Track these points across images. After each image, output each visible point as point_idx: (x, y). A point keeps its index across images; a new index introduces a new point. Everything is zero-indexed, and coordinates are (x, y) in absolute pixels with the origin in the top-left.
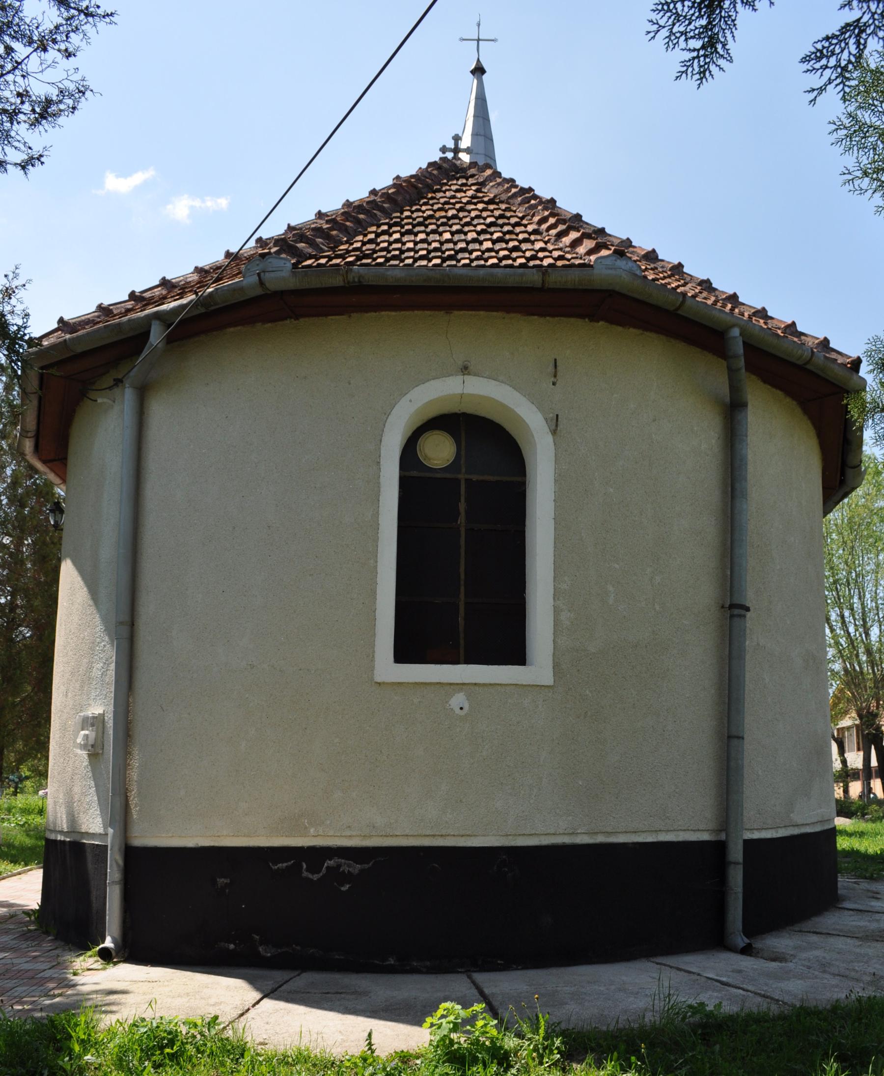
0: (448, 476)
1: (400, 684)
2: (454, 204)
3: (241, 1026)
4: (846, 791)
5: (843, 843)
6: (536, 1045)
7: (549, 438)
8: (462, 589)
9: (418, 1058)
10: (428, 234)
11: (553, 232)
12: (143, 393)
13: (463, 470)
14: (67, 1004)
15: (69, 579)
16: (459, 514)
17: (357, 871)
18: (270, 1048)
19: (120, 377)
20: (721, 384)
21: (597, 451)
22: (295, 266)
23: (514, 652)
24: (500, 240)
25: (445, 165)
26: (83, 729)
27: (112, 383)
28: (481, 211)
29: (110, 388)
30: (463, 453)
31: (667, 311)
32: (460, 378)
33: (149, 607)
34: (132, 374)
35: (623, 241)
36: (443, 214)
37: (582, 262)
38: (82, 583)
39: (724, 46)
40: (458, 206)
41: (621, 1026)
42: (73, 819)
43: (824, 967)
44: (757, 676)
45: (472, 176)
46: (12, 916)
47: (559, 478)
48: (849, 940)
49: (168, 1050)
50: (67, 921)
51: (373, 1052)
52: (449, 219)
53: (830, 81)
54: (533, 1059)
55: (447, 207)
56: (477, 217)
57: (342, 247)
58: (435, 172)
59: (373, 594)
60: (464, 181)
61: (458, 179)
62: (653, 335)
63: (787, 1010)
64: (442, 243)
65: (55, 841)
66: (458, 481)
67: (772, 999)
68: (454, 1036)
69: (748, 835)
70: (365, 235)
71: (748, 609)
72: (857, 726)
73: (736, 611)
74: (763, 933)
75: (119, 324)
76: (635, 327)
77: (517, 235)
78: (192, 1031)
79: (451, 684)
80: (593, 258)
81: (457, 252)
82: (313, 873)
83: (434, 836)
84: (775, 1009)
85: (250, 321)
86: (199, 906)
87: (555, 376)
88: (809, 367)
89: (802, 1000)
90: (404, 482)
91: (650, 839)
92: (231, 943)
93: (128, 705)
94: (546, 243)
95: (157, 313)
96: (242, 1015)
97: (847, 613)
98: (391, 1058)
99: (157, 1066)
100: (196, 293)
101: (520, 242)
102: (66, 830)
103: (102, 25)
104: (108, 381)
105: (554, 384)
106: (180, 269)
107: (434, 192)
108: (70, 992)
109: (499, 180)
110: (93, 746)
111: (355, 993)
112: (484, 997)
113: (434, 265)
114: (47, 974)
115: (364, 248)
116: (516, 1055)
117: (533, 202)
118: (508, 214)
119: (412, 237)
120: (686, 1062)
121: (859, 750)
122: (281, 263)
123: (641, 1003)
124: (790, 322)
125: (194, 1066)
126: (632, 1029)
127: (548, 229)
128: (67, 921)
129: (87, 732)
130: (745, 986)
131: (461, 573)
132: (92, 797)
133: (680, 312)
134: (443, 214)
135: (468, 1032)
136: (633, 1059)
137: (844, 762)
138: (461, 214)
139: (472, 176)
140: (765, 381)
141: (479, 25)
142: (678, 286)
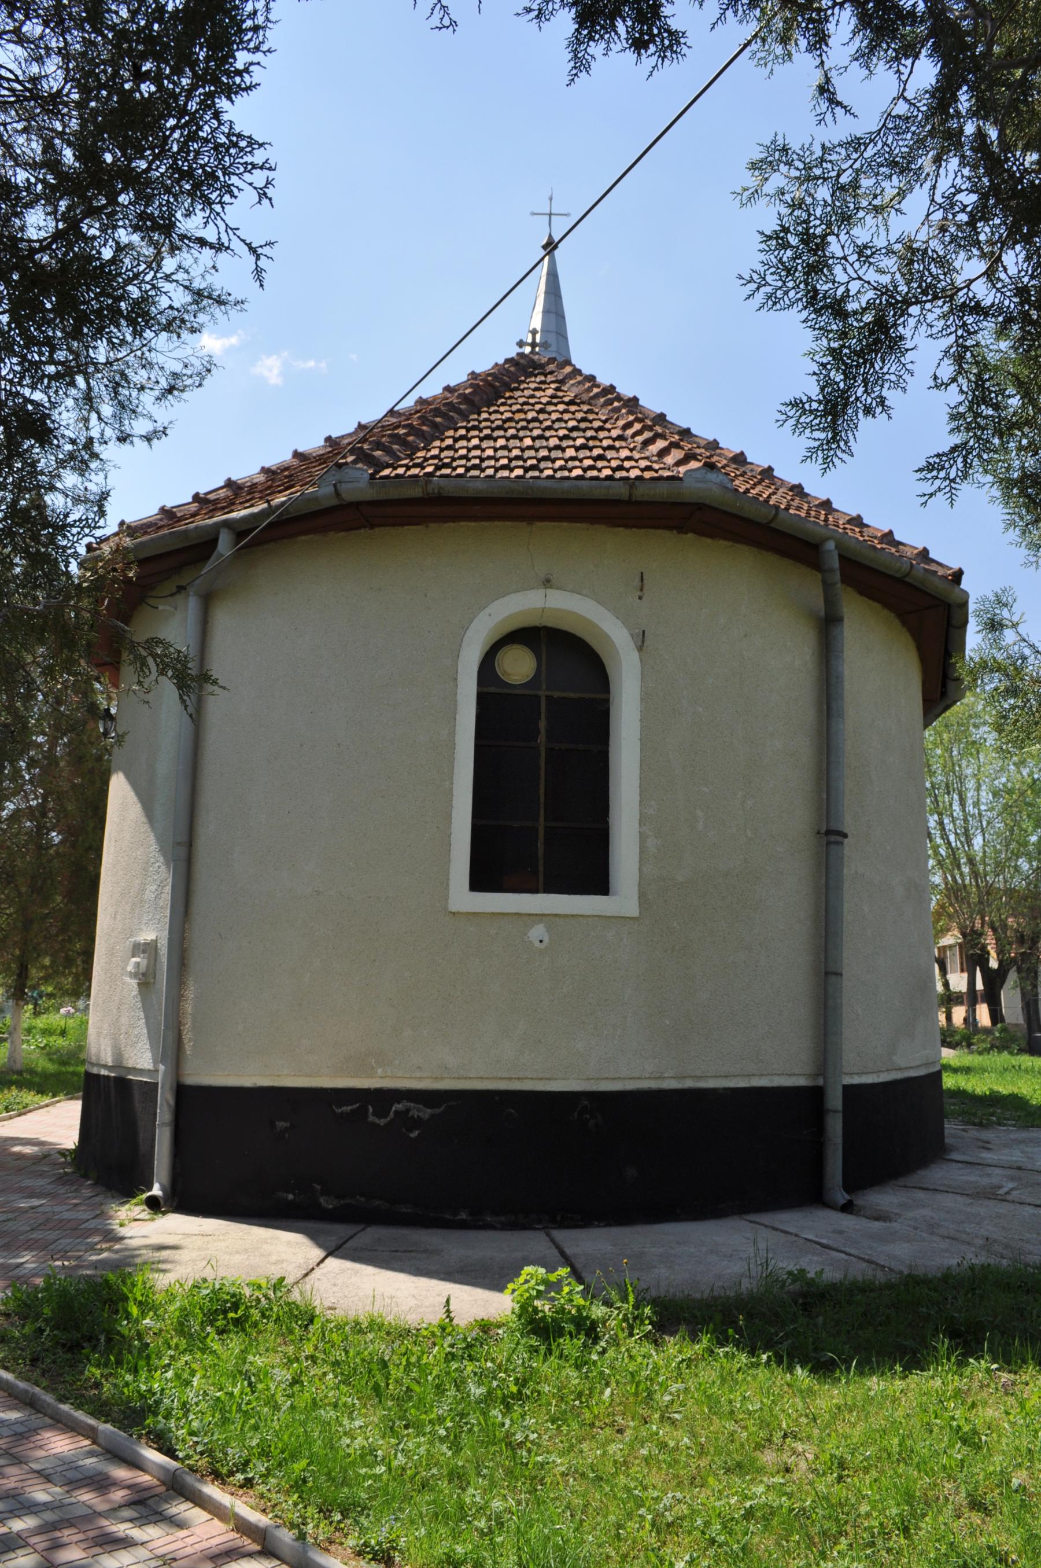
0: (527, 692)
1: (476, 914)
2: (533, 405)
3: (308, 1287)
4: (949, 1018)
5: (949, 1082)
6: (625, 1315)
7: (635, 655)
8: (542, 811)
9: (499, 1327)
10: (508, 439)
11: (639, 439)
12: (207, 601)
13: (544, 687)
14: (117, 1260)
15: (120, 791)
16: (539, 732)
17: (427, 1116)
18: (339, 1313)
19: (183, 583)
20: (816, 597)
21: (689, 677)
22: (372, 477)
23: (596, 879)
24: (583, 447)
25: (522, 361)
26: (133, 956)
27: (174, 590)
28: (562, 413)
29: (172, 595)
30: (544, 668)
31: (759, 524)
32: (541, 592)
33: (208, 829)
34: (197, 582)
35: (709, 443)
36: (522, 416)
37: (670, 474)
38: (135, 799)
39: (846, 443)
40: (538, 407)
41: (716, 1293)
42: (118, 1055)
43: (932, 1227)
44: (857, 907)
45: (551, 373)
46: (46, 1156)
47: (646, 697)
48: (958, 1198)
49: (231, 1315)
50: (107, 1161)
51: (451, 1320)
52: (529, 422)
53: (939, 489)
54: (623, 1330)
55: (526, 408)
56: (559, 420)
57: (419, 454)
58: (512, 369)
59: (449, 817)
60: (543, 378)
61: (536, 376)
62: (745, 548)
63: (894, 1278)
64: (523, 450)
65: (98, 1076)
66: (538, 697)
67: (877, 1264)
68: (537, 1303)
69: (848, 1080)
70: (442, 440)
71: (845, 836)
72: (960, 945)
73: (833, 838)
74: (865, 1188)
75: (185, 531)
76: (725, 539)
77: (601, 441)
78: (257, 1293)
79: (530, 915)
80: (682, 469)
81: (539, 460)
82: (380, 1118)
83: (510, 1079)
84: (881, 1277)
85: (324, 530)
86: (254, 1153)
87: (641, 590)
88: (907, 579)
89: (910, 1267)
90: (482, 699)
91: (742, 1083)
92: (288, 1192)
93: (184, 931)
94: (631, 450)
95: (225, 521)
96: (306, 1275)
97: (946, 821)
98: (470, 1327)
99: (221, 1332)
100: (268, 502)
101: (604, 449)
102: (110, 1064)
103: (233, 313)
104: (170, 586)
105: (640, 598)
106: (246, 468)
107: (512, 390)
108: (117, 1247)
109: (579, 378)
110: (143, 974)
111: (425, 1251)
112: (567, 1261)
113: (517, 477)
114: (92, 1224)
115: (443, 455)
116: (604, 1323)
117: (616, 404)
118: (591, 417)
119: (491, 443)
120: (787, 1336)
121: (962, 971)
122: (358, 474)
123: (736, 1268)
124: (887, 530)
125: (260, 1332)
126: (728, 1298)
127: (634, 435)
128: (107, 1161)
129: (138, 960)
130: (847, 1250)
131: (541, 796)
132: (141, 1029)
133: (773, 525)
134: (522, 416)
135: (552, 1300)
136: (731, 1331)
137: (946, 984)
138: (542, 417)
139: (551, 373)
140: (861, 593)
141: (551, 199)
142: (769, 497)
